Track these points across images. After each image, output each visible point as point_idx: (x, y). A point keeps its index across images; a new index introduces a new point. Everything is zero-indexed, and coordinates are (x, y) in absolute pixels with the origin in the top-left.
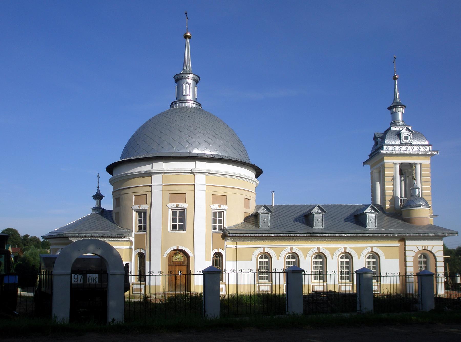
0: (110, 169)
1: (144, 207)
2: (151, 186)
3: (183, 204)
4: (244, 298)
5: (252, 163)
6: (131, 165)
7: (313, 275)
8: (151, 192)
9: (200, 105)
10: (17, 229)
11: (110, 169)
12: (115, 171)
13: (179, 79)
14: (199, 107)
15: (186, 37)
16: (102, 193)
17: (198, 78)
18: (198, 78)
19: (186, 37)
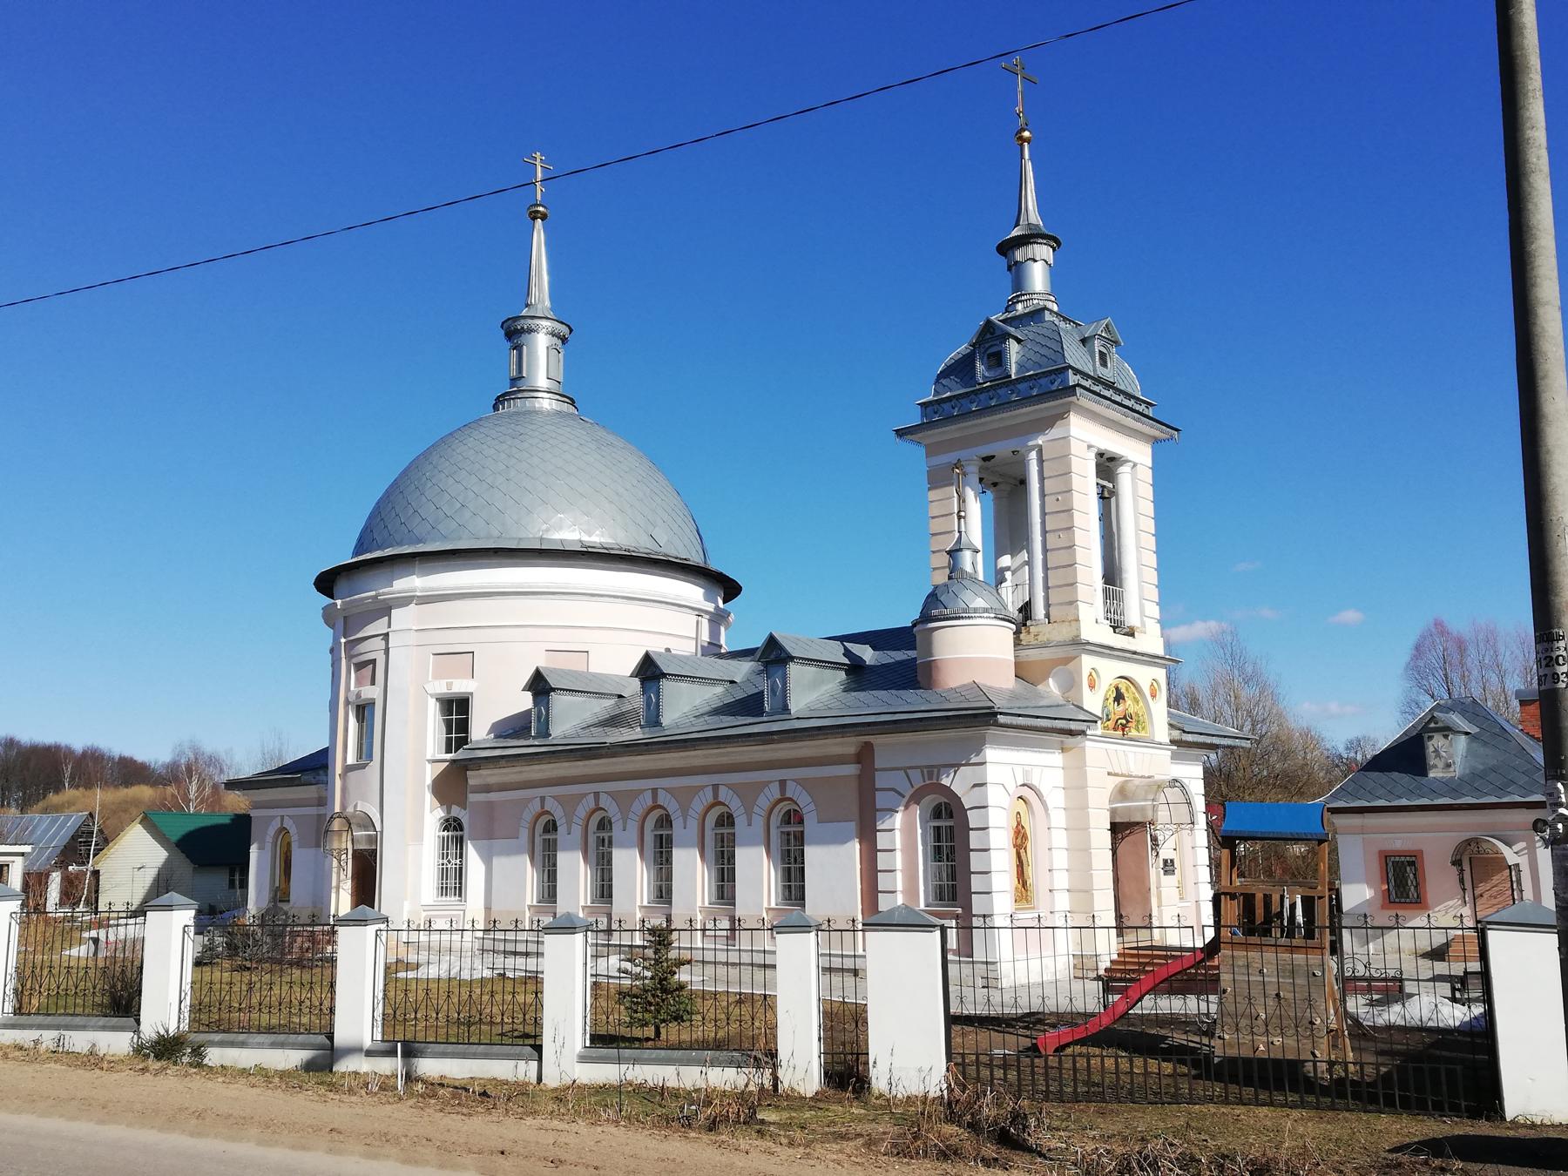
0: (327, 583)
1: (369, 692)
2: (387, 635)
3: (465, 681)
4: (1474, 1023)
5: (715, 565)
6: (381, 573)
7: (1460, 932)
8: (387, 651)
9: (573, 402)
10: (89, 744)
11: (327, 583)
12: (341, 585)
13: (515, 333)
14: (572, 409)
15: (534, 216)
16: (758, 641)
17: (564, 330)
18: (564, 330)
19: (1023, 140)
